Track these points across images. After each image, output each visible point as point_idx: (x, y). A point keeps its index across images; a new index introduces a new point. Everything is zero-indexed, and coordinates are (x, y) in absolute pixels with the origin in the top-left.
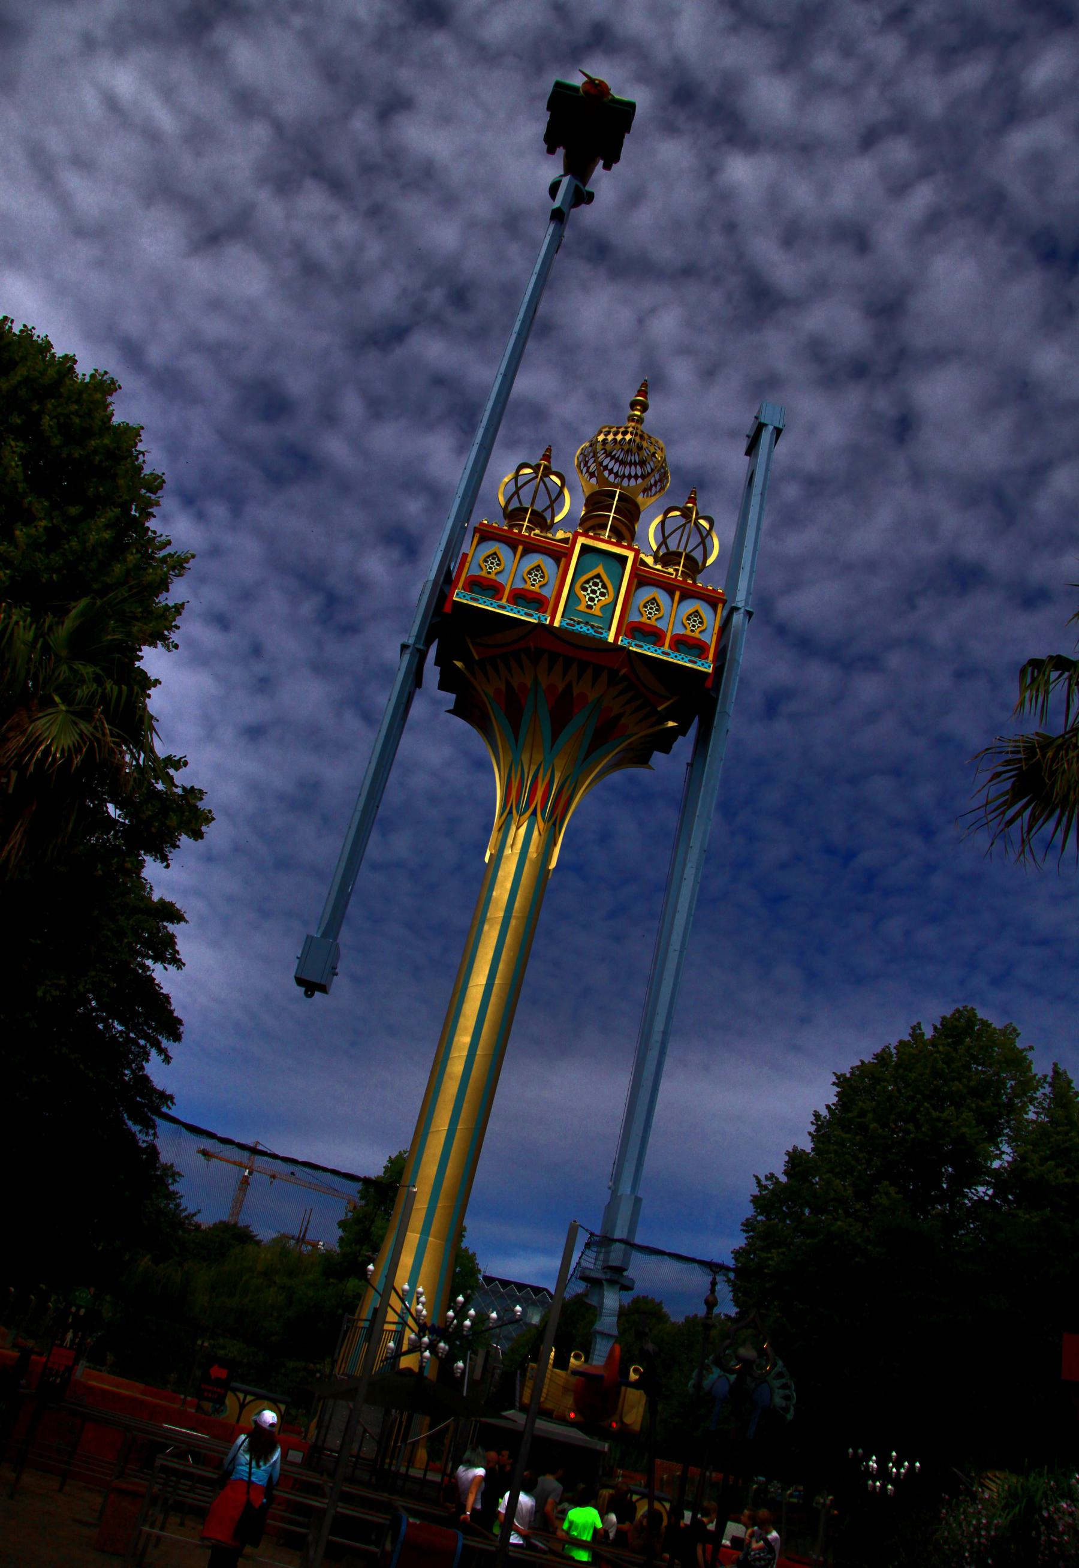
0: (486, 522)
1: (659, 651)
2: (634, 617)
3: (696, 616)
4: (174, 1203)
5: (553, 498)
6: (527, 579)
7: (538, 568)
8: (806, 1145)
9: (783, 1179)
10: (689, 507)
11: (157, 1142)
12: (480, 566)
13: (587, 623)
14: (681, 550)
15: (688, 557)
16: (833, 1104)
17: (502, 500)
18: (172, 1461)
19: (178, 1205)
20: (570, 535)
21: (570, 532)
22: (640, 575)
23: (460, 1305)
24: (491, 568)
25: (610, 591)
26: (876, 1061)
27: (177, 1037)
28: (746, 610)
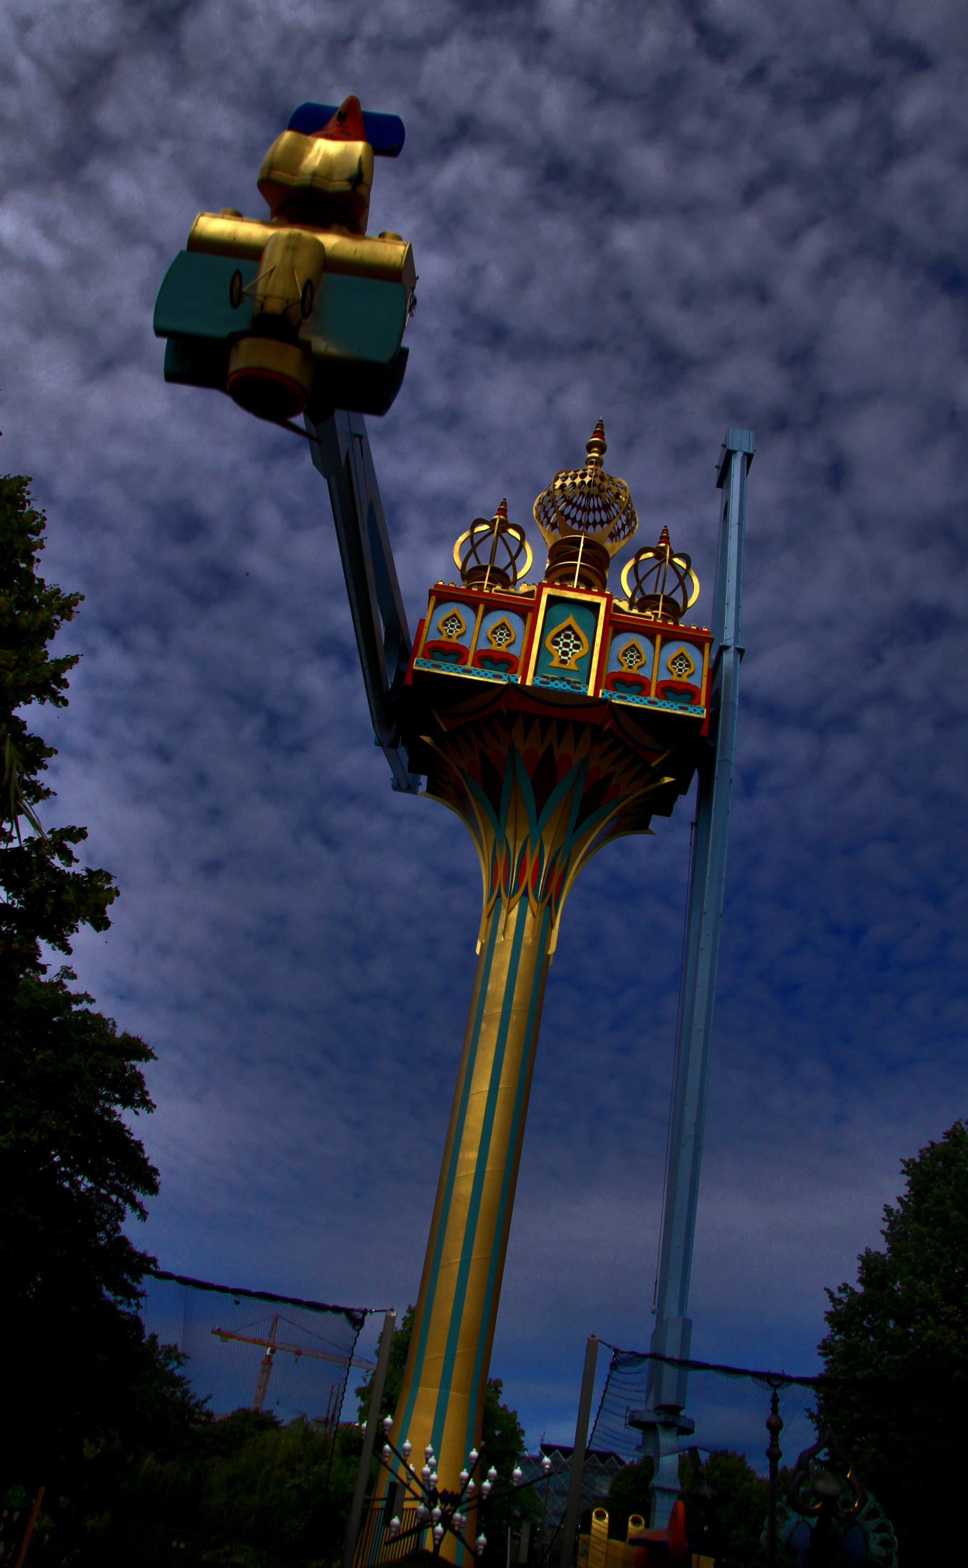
0: (441, 583)
1: (645, 701)
2: (613, 667)
3: (681, 660)
4: (182, 1389)
5: (514, 554)
6: (493, 640)
7: (503, 626)
8: (881, 1246)
9: (859, 1288)
10: (662, 547)
13: (562, 679)
14: (658, 593)
15: (667, 600)
16: (905, 1196)
17: (458, 562)
19: (185, 1392)
20: (535, 588)
21: (534, 584)
22: (614, 622)
24: (451, 631)
25: (584, 644)
26: (947, 1140)
27: (153, 1189)
28: (736, 648)
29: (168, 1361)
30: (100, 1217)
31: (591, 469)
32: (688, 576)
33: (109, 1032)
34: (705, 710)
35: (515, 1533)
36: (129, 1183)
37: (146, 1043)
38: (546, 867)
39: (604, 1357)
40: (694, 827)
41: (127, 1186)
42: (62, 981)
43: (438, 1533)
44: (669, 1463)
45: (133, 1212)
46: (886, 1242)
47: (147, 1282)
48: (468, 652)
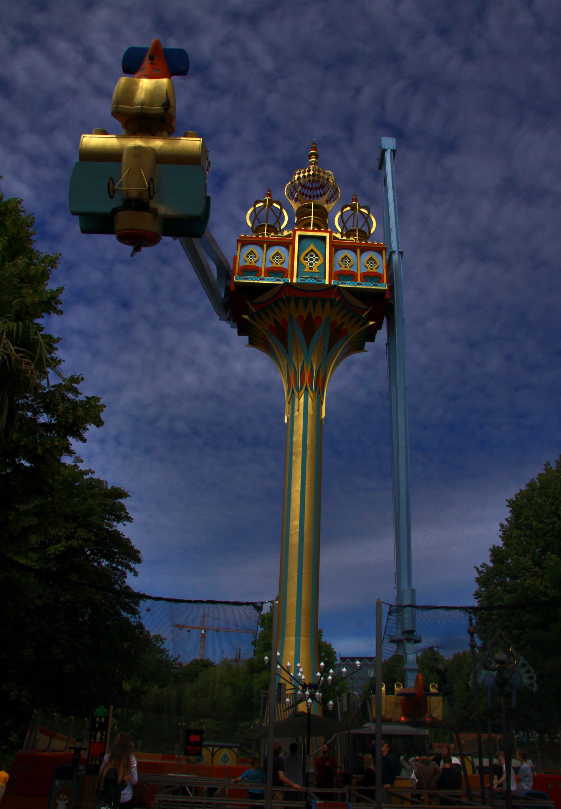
0: (243, 236)
1: (355, 284)
2: (337, 268)
3: (371, 260)
4: (165, 654)
7: (277, 254)
8: (500, 543)
9: (491, 565)
11: (142, 621)
12: (245, 260)
13: (312, 278)
14: (355, 228)
16: (509, 518)
17: (250, 224)
18: (165, 797)
19: (167, 655)
23: (323, 668)
25: (320, 258)
26: (528, 488)
27: (139, 561)
29: (157, 642)
30: (114, 578)
31: (313, 167)
32: (369, 218)
33: (104, 487)
34: (387, 285)
35: (340, 698)
36: (126, 559)
37: (123, 489)
38: (315, 375)
39: (385, 609)
40: (387, 346)
41: (125, 561)
42: (76, 464)
43: (309, 703)
44: (411, 657)
45: (130, 573)
46: (502, 541)
47: (143, 605)
48: (261, 270)
